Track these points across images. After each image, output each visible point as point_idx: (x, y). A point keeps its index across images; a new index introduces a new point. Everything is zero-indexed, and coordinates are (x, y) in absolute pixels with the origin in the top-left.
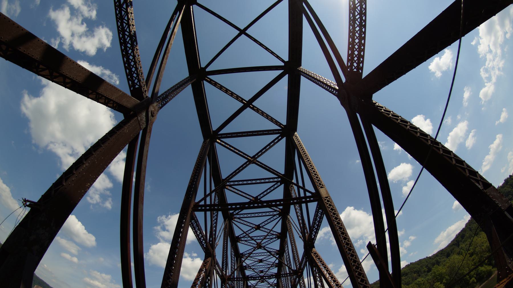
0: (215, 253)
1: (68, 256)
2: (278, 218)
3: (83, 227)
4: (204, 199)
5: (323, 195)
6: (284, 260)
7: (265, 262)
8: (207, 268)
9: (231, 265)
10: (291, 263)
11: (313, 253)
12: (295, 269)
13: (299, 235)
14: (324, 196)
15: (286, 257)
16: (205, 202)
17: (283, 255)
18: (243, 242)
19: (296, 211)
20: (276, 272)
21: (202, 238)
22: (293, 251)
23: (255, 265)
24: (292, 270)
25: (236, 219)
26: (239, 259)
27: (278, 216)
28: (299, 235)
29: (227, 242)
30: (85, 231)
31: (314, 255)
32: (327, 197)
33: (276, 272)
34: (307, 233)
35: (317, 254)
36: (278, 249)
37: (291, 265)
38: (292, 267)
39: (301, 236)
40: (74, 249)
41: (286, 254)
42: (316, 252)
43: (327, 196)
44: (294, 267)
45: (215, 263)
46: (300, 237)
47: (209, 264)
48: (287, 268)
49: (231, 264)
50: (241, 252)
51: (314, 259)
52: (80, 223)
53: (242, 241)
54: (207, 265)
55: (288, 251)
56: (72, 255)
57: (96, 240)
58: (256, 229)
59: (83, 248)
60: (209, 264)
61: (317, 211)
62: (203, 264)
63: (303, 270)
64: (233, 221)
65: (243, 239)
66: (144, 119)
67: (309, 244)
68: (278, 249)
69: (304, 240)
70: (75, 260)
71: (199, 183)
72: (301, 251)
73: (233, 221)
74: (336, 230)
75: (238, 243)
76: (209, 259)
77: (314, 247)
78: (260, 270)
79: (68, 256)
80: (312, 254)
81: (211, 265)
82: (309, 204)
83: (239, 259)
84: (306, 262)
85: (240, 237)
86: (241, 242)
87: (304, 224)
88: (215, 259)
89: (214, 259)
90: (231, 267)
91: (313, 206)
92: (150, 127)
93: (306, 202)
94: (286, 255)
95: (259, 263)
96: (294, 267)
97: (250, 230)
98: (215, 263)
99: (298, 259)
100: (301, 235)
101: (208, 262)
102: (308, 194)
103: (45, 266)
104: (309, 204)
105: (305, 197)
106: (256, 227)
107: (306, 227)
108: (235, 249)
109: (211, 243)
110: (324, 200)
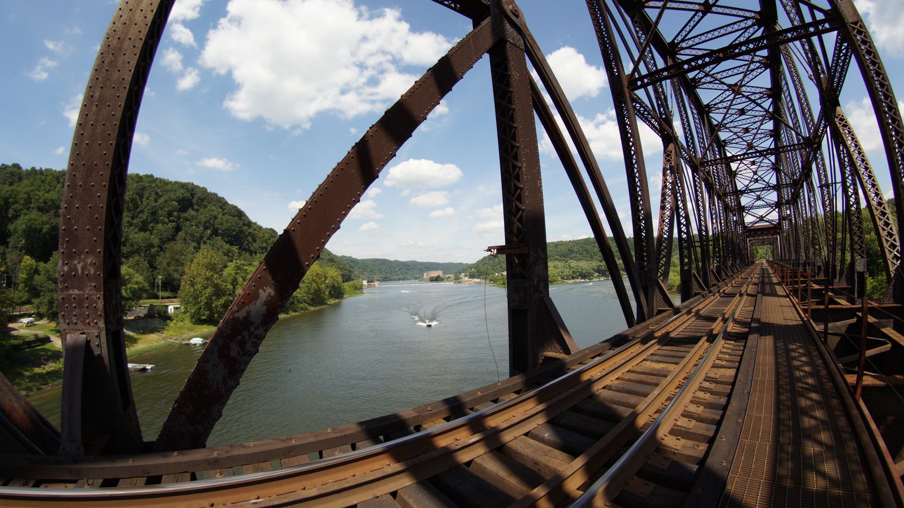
0: (676, 133)
1: (438, 213)
2: (757, 30)
3: (431, 162)
4: (636, 69)
5: (848, 18)
6: (784, 108)
7: (749, 113)
8: (673, 164)
9: (696, 129)
10: (797, 117)
11: (837, 117)
12: (808, 136)
13: (807, 72)
14: (850, 21)
15: (786, 99)
16: (639, 73)
17: (780, 98)
18: (705, 85)
19: (789, 17)
20: (772, 128)
21: (646, 113)
22: (799, 99)
23: (725, 98)
24: (802, 137)
25: (682, 52)
26: (705, 115)
27: (756, 27)
28: (807, 72)
29: (683, 101)
30: (438, 166)
31: (840, 124)
32: (856, 23)
33: (772, 128)
34: (823, 72)
35: (846, 122)
36: (769, 86)
37: (798, 121)
38: (801, 132)
39: (811, 75)
40: (439, 198)
41: (784, 94)
42: (842, 116)
43: (856, 20)
44: (805, 133)
45: (679, 148)
46: (810, 78)
47: (673, 155)
48: (793, 133)
49: (695, 126)
50: (705, 102)
51: (836, 125)
52: (423, 161)
53: (683, 49)
54: (671, 158)
55: (789, 93)
56: (442, 207)
57: (459, 166)
58: (704, 14)
59: (449, 188)
60: (673, 155)
61: (838, 49)
62: (666, 158)
63: (820, 138)
64: (677, 56)
65: (684, 45)
66: (515, 33)
67: (830, 100)
68: (769, 86)
69: (819, 85)
70: (450, 211)
71: (614, 38)
72: (816, 108)
73: (677, 56)
74: (874, 87)
75: (697, 89)
76: (671, 147)
77: (839, 105)
78: (738, 110)
79: (438, 213)
80: (836, 120)
81: (677, 155)
82: (824, 36)
83: (705, 115)
84: (825, 127)
85: (676, 41)
86: (701, 86)
87: (815, 54)
88: (679, 143)
89: (677, 144)
90: (697, 132)
91: (831, 39)
92: (529, 35)
93: (819, 34)
94: (785, 96)
95: (740, 115)
96: (805, 133)
97: (691, 20)
98: (679, 148)
99: (812, 120)
100: (811, 73)
101: (671, 152)
102: (820, 16)
103: (420, 243)
104: (824, 36)
105: (815, 23)
106: (702, 8)
107: (819, 59)
108: (696, 101)
109: (664, 116)
110: (850, 29)
